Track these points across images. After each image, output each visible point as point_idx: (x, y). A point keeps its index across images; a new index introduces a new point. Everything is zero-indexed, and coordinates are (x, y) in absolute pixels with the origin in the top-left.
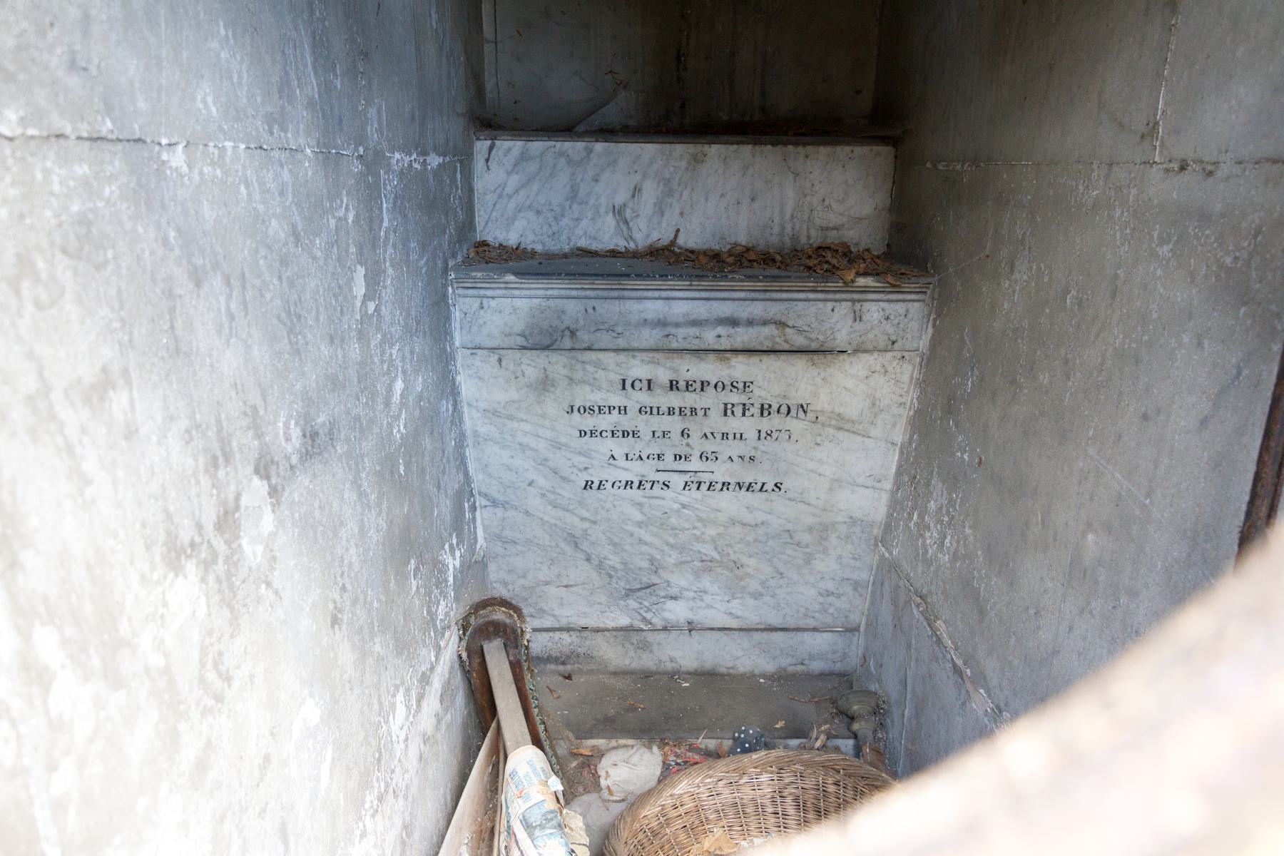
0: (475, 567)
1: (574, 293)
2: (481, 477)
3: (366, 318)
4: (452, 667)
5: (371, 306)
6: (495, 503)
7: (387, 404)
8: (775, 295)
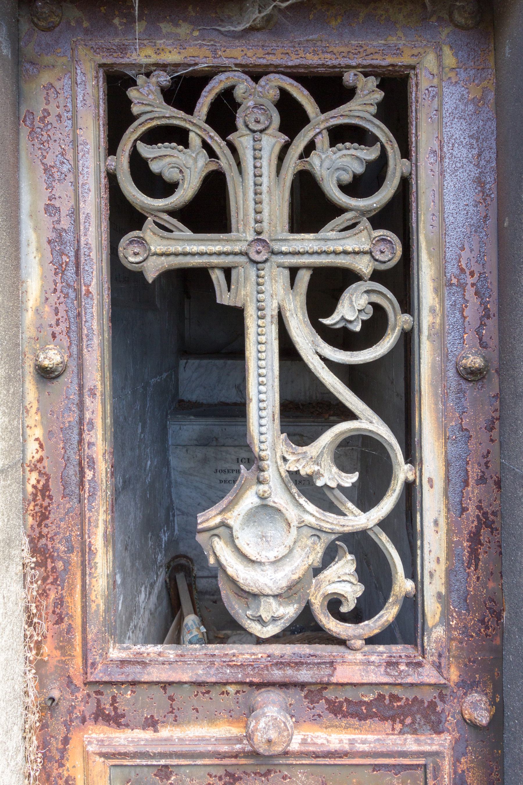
0: (173, 542)
1: (217, 423)
2: (177, 501)
3: (141, 439)
4: (162, 586)
5: (142, 435)
6: (183, 513)
7: (145, 470)
8: (298, 424)
